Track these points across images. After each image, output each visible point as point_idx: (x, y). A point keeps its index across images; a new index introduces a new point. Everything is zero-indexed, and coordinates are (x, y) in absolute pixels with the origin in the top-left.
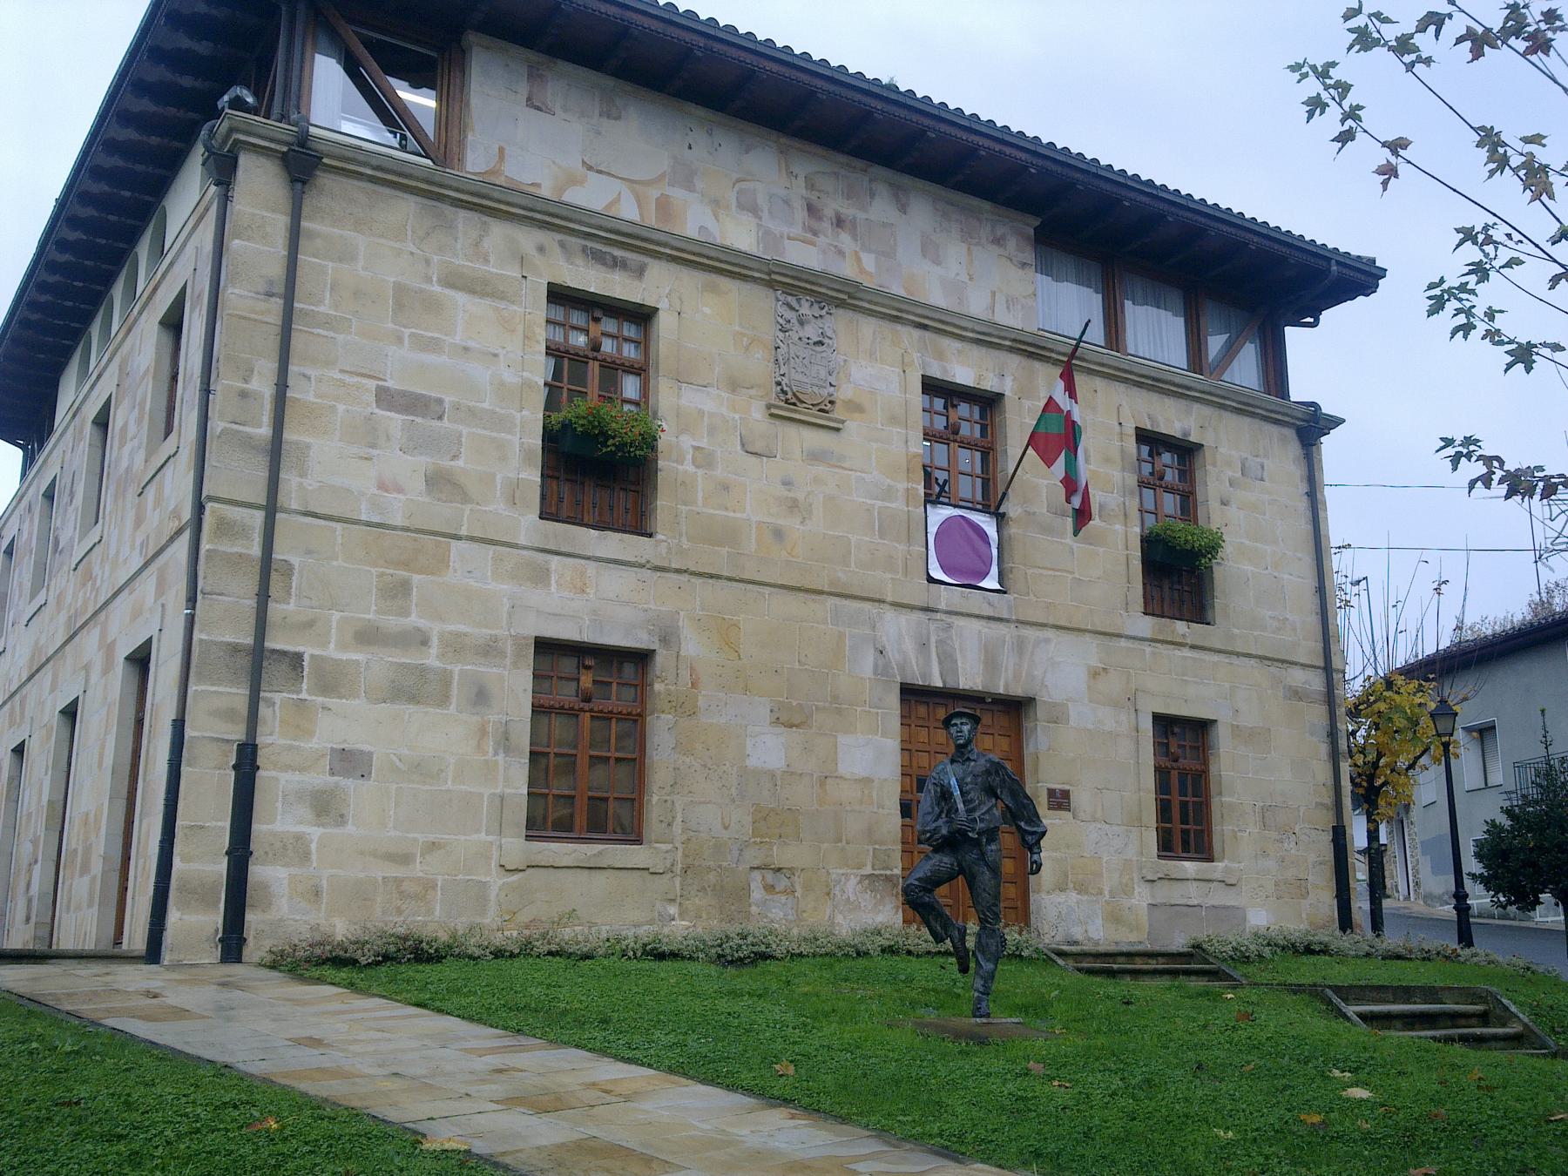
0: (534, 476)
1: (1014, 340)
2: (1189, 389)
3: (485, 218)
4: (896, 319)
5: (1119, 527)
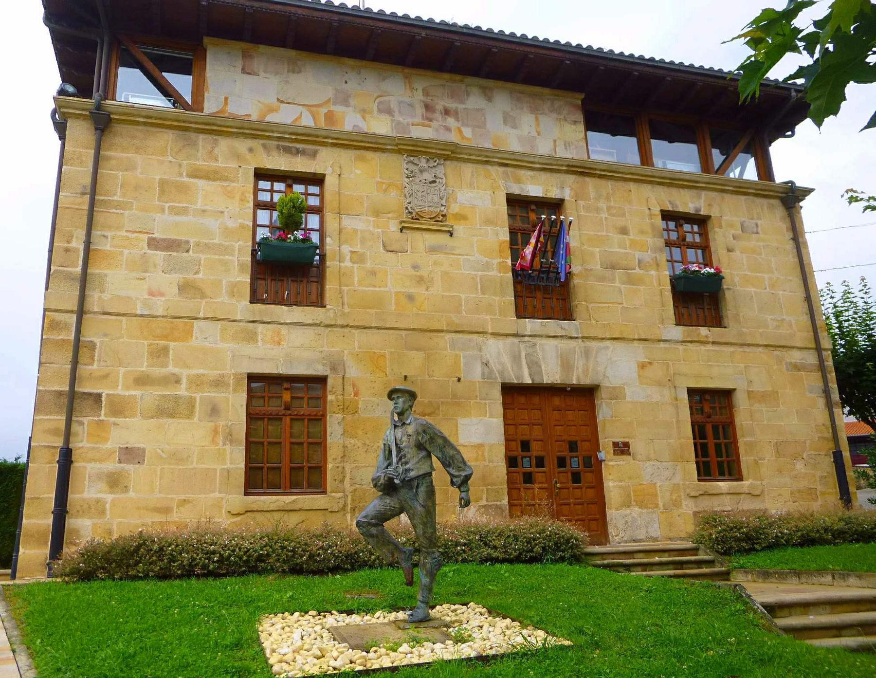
1: (568, 166)
2: (145, 124)
3: (215, 137)
4: (487, 162)
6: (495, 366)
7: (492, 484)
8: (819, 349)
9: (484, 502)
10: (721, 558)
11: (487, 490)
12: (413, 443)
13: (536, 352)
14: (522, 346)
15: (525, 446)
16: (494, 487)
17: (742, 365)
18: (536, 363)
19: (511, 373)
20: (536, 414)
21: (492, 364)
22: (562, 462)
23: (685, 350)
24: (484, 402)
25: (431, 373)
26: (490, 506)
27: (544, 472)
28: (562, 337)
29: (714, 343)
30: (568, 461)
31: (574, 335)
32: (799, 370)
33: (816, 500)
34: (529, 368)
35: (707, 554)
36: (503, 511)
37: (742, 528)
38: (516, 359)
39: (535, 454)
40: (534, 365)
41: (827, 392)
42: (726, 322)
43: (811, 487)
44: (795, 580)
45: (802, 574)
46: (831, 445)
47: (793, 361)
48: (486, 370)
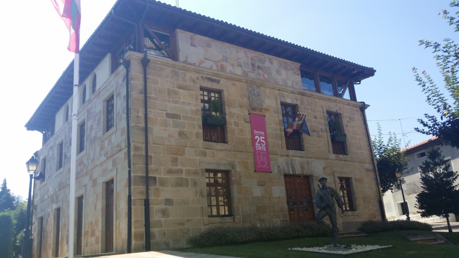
0: (201, 131)
5: (325, 134)
9: (282, 219)
21: (280, 166)
28: (301, 157)
29: (344, 161)
34: (292, 168)
38: (287, 164)
40: (293, 167)
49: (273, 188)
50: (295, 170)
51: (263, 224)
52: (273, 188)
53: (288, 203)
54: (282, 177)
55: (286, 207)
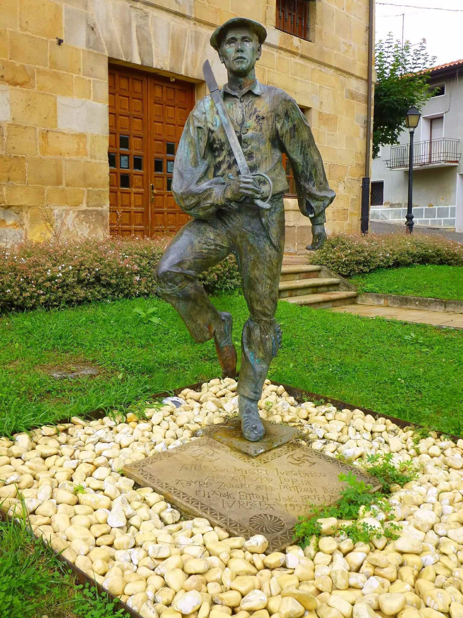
6: (104, 36)
7: (94, 186)
8: (369, 81)
9: (84, 207)
10: (345, 280)
11: (88, 191)
12: (267, 134)
13: (146, 25)
14: (133, 14)
15: (124, 142)
16: (96, 189)
17: (318, 85)
18: (147, 40)
19: (120, 46)
20: (137, 104)
21: (99, 28)
22: (138, 164)
23: (279, 58)
24: (88, 78)
25: (24, 25)
26: (91, 211)
27: (142, 175)
28: (176, 14)
29: (302, 57)
30: (164, 164)
31: (187, 13)
32: (353, 99)
33: (345, 219)
34: (139, 44)
35: (331, 276)
36: (104, 218)
37: (363, 251)
38: (126, 27)
39: (134, 152)
40: (144, 42)
41: (368, 122)
42: (311, 35)
43: (345, 208)
44: (440, 308)
45: (450, 303)
46: (362, 172)
47: (351, 89)
48: (92, 37)
49: (61, 100)
50: (150, 53)
51: (362, 405)
52: (61, 100)
53: (112, 161)
54: (103, 71)
55: (104, 168)
